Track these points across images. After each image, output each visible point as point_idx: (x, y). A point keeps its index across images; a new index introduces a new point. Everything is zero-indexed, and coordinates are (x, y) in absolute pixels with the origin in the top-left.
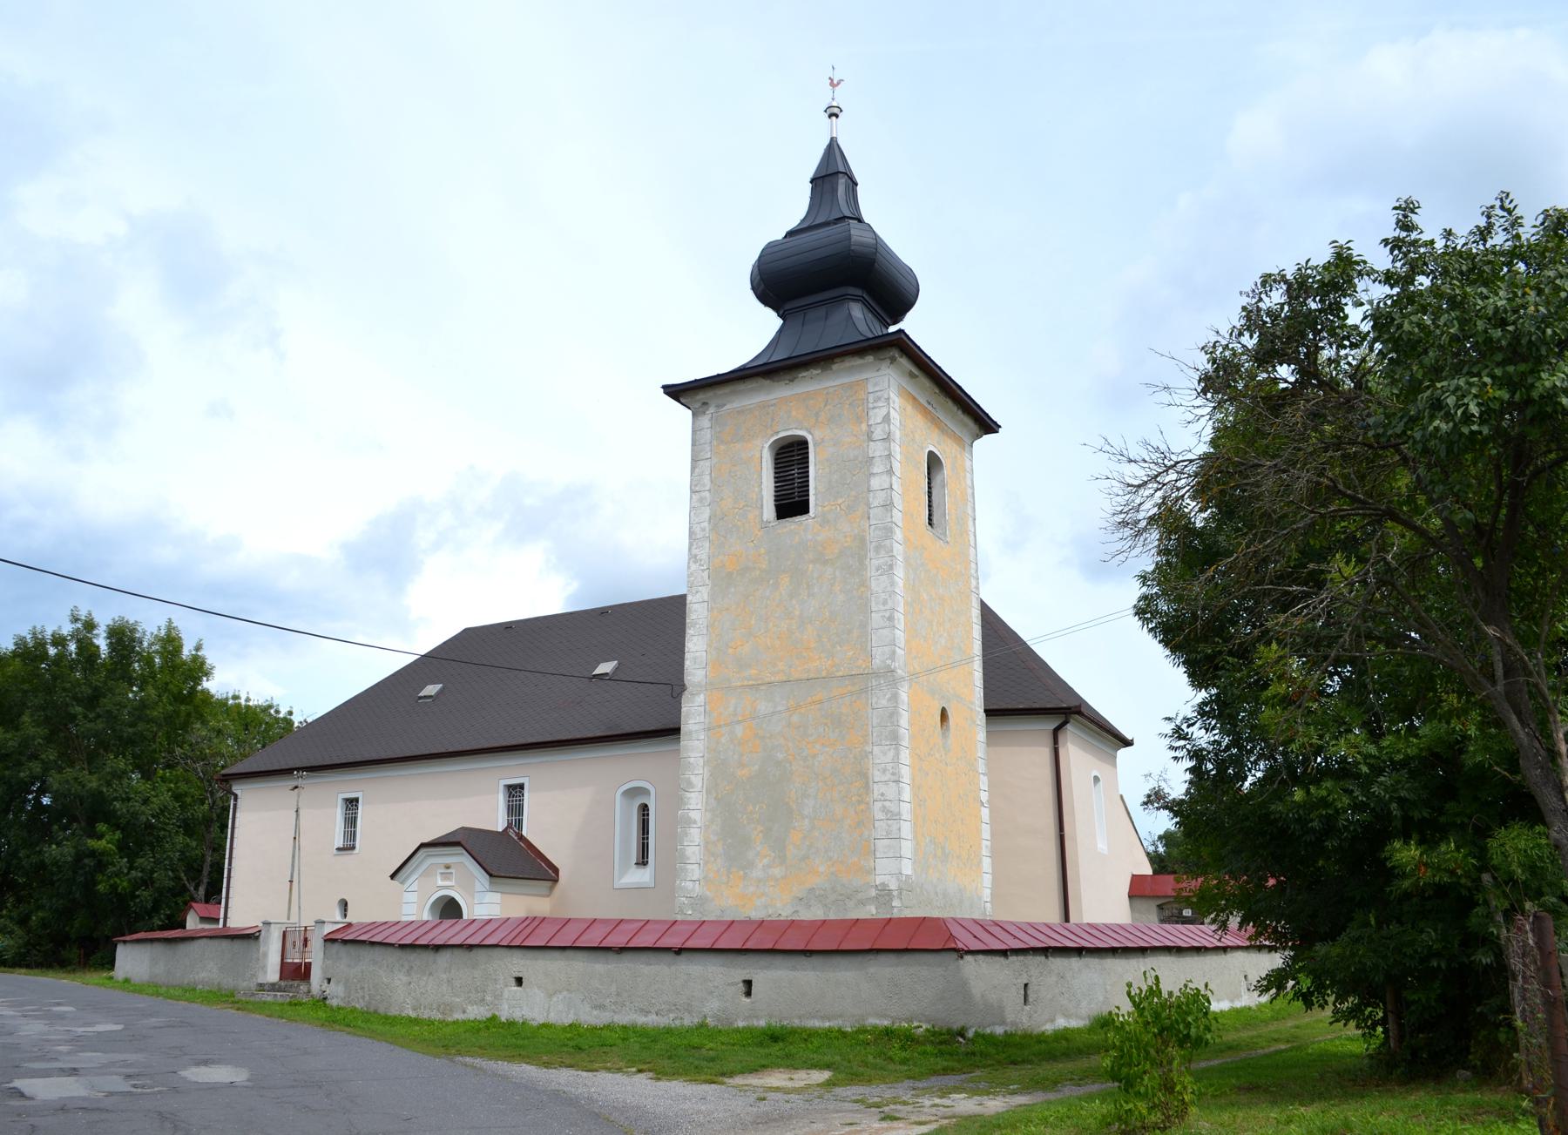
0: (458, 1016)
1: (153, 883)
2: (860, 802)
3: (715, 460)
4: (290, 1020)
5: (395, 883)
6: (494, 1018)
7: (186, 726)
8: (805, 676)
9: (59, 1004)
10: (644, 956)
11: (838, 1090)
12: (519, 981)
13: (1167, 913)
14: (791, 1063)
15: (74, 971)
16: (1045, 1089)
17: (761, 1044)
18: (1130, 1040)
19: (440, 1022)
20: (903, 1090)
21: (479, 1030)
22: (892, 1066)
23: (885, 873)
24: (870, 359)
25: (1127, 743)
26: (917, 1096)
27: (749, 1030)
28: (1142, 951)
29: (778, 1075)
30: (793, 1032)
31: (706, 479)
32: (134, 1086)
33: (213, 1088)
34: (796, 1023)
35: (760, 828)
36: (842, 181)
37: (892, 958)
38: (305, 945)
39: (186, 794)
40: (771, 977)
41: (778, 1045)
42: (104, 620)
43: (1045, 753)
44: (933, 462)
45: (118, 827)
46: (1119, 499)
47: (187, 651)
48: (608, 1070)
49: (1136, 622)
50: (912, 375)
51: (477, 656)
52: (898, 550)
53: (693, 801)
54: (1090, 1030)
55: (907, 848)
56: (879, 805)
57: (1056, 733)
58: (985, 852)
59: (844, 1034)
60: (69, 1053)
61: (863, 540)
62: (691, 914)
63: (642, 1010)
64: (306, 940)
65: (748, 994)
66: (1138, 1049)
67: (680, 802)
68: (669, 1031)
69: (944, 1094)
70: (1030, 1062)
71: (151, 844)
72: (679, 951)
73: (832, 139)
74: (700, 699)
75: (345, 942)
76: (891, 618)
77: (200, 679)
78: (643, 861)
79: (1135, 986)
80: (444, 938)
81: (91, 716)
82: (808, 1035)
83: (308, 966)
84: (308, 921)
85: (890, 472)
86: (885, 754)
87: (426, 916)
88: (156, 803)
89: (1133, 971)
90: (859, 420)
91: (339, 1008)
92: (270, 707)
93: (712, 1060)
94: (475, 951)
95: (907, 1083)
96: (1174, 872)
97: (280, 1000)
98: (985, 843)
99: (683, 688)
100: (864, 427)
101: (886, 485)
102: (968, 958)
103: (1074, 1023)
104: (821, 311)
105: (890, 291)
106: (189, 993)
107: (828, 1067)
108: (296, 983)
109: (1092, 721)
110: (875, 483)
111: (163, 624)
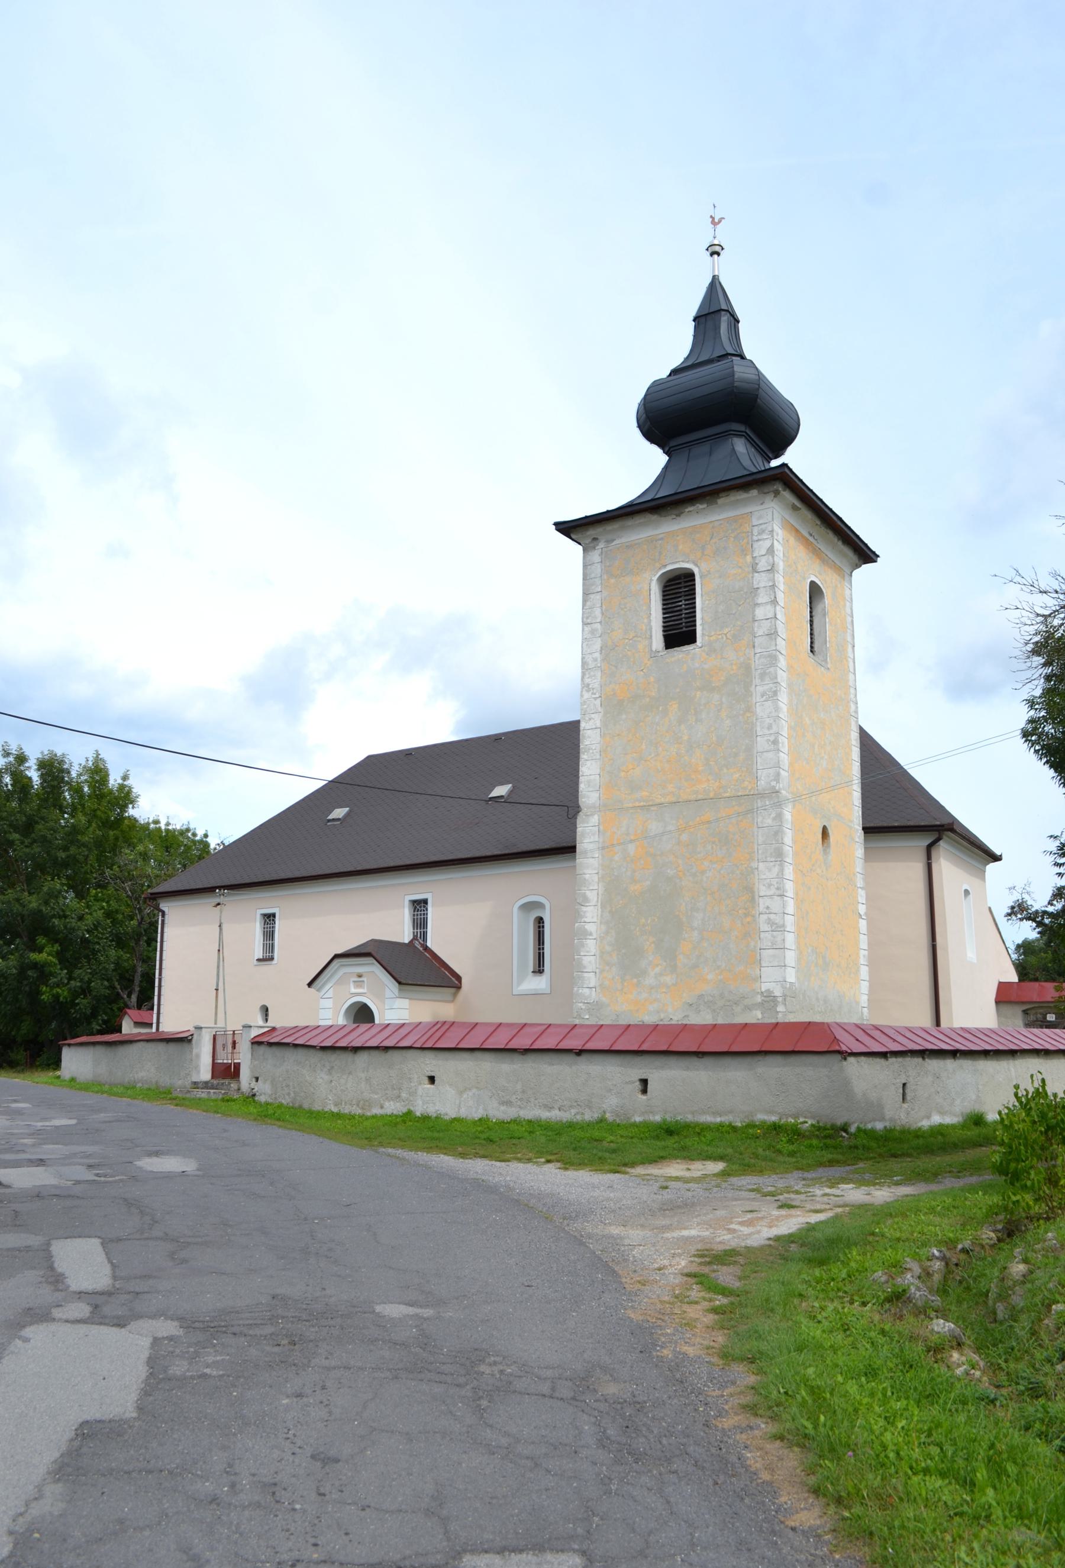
0: (376, 1111)
1: (90, 991)
2: (746, 915)
4: (224, 1114)
5: (312, 990)
6: (409, 1113)
7: (115, 849)
8: (693, 797)
9: (15, 1101)
10: (547, 1058)
11: (734, 1180)
12: (432, 1080)
13: (1032, 1018)
14: (687, 1154)
15: (23, 1071)
16: (926, 1180)
17: (657, 1138)
18: (1019, 1138)
19: (360, 1116)
20: (794, 1180)
21: (396, 1124)
22: (781, 1158)
23: (769, 981)
24: (754, 492)
25: (996, 858)
26: (809, 1186)
27: (646, 1124)
28: (1012, 1053)
29: (677, 1166)
30: (687, 1126)
31: (598, 612)
32: (97, 1175)
33: (168, 1176)
34: (689, 1118)
36: (725, 319)
37: (779, 1059)
38: (234, 1047)
39: (117, 911)
40: (666, 1077)
41: (673, 1138)
42: (34, 756)
43: (918, 868)
44: (815, 592)
45: (56, 941)
46: (1027, 628)
47: (114, 780)
48: (519, 1160)
49: (1021, 747)
50: (794, 508)
51: (379, 780)
52: (782, 676)
53: (588, 915)
54: (964, 1126)
55: (791, 957)
56: (764, 917)
57: (929, 848)
58: (862, 961)
59: (735, 1129)
60: (34, 1145)
61: (748, 668)
62: (588, 1019)
64: (234, 1043)
65: (644, 1091)
66: (1026, 1146)
67: (576, 915)
68: (571, 1125)
69: (833, 1183)
70: (909, 1155)
71: (87, 957)
72: (580, 1053)
73: (714, 277)
74: (595, 819)
75: (270, 1044)
76: (775, 742)
77: (126, 806)
79: (1022, 1087)
80: (358, 1039)
81: (27, 841)
82: (700, 1130)
83: (237, 1066)
84: (238, 1027)
85: (774, 602)
86: (770, 870)
87: (341, 1021)
88: (89, 920)
89: (1022, 1074)
90: (744, 552)
91: (267, 1104)
92: (188, 830)
93: (614, 1151)
95: (797, 1174)
96: (1036, 980)
97: (214, 1097)
98: (862, 953)
99: (577, 809)
100: (749, 559)
101: (771, 615)
102: (851, 1059)
103: (948, 1120)
104: (705, 448)
105: (766, 423)
106: (129, 1090)
107: (721, 1158)
108: (227, 1081)
109: (963, 837)
110: (760, 613)
111: (91, 756)
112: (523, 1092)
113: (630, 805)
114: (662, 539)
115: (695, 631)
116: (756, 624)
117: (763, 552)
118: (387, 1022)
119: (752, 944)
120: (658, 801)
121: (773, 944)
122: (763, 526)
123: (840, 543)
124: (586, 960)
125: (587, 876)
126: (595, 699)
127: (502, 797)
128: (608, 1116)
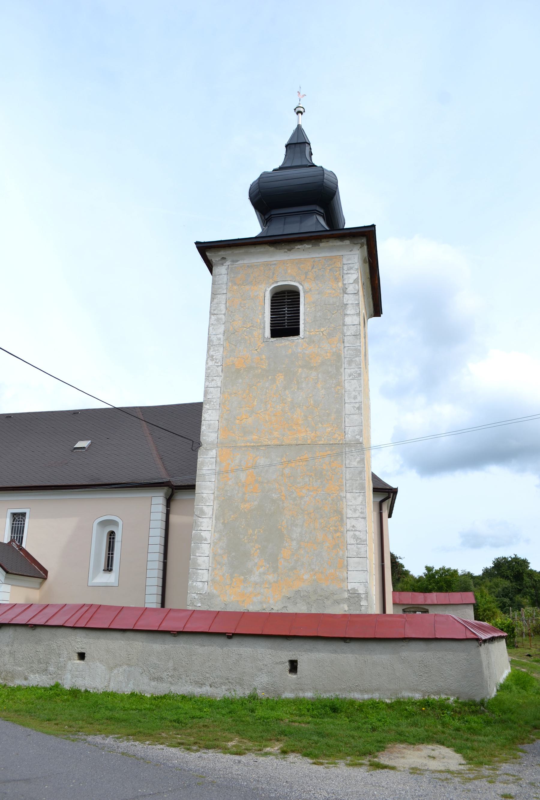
0: (19, 682)
2: (336, 531)
3: (229, 295)
8: (295, 442)
12: (82, 656)
24: (347, 242)
27: (297, 702)
31: (223, 307)
35: (257, 546)
40: (315, 660)
53: (203, 524)
62: (199, 606)
63: (197, 683)
78: (109, 568)
86: (355, 499)
90: (337, 280)
94: (38, 630)
99: (199, 444)
100: (340, 284)
104: (297, 218)
112: (175, 669)
113: (243, 444)
114: (275, 264)
115: (299, 328)
116: (346, 327)
117: (352, 281)
118: (62, 602)
119: (341, 553)
120: (265, 443)
121: (357, 553)
122: (351, 265)
123: (371, 297)
124: (200, 560)
125: (204, 495)
126: (218, 366)
127: (84, 448)
128: (261, 694)
